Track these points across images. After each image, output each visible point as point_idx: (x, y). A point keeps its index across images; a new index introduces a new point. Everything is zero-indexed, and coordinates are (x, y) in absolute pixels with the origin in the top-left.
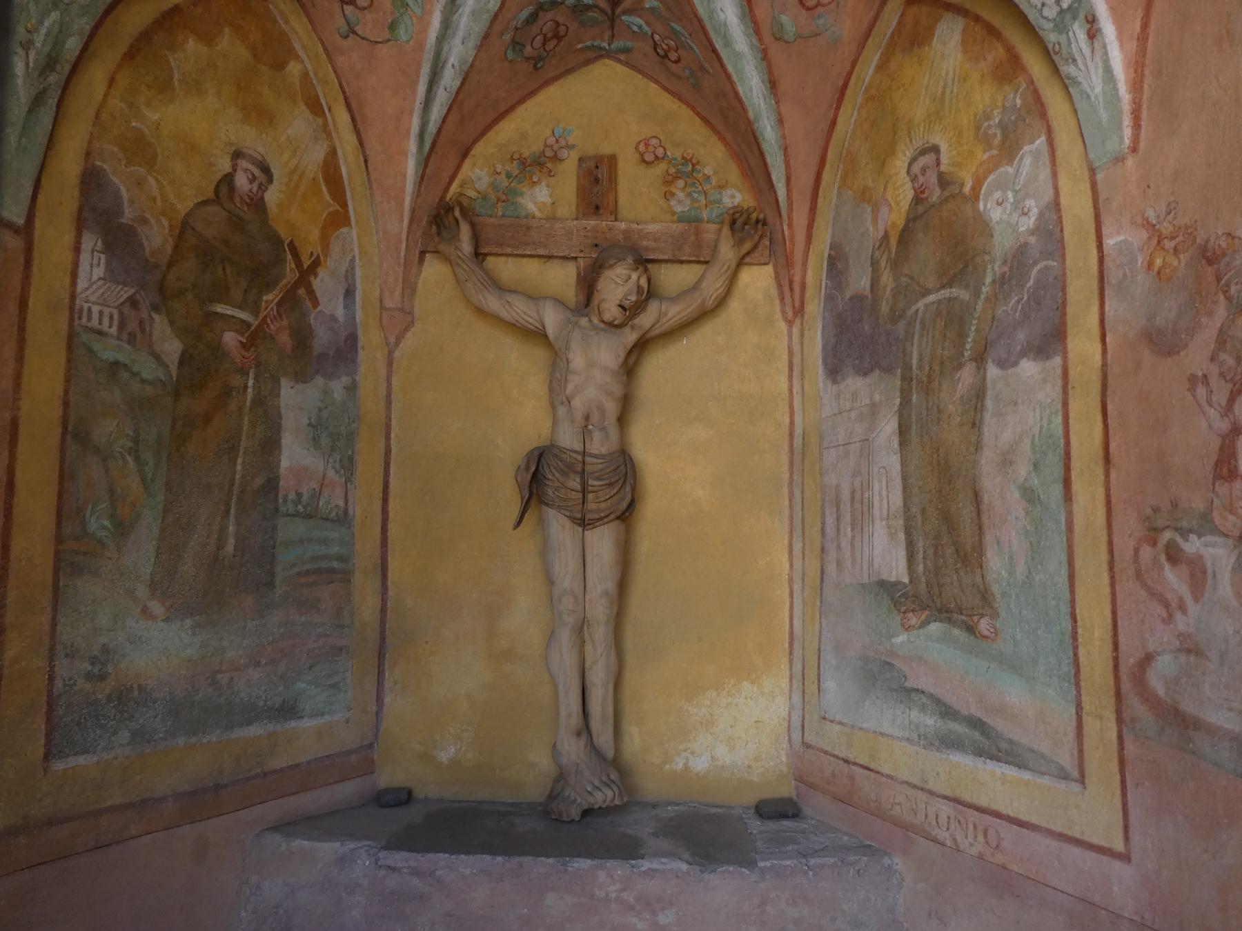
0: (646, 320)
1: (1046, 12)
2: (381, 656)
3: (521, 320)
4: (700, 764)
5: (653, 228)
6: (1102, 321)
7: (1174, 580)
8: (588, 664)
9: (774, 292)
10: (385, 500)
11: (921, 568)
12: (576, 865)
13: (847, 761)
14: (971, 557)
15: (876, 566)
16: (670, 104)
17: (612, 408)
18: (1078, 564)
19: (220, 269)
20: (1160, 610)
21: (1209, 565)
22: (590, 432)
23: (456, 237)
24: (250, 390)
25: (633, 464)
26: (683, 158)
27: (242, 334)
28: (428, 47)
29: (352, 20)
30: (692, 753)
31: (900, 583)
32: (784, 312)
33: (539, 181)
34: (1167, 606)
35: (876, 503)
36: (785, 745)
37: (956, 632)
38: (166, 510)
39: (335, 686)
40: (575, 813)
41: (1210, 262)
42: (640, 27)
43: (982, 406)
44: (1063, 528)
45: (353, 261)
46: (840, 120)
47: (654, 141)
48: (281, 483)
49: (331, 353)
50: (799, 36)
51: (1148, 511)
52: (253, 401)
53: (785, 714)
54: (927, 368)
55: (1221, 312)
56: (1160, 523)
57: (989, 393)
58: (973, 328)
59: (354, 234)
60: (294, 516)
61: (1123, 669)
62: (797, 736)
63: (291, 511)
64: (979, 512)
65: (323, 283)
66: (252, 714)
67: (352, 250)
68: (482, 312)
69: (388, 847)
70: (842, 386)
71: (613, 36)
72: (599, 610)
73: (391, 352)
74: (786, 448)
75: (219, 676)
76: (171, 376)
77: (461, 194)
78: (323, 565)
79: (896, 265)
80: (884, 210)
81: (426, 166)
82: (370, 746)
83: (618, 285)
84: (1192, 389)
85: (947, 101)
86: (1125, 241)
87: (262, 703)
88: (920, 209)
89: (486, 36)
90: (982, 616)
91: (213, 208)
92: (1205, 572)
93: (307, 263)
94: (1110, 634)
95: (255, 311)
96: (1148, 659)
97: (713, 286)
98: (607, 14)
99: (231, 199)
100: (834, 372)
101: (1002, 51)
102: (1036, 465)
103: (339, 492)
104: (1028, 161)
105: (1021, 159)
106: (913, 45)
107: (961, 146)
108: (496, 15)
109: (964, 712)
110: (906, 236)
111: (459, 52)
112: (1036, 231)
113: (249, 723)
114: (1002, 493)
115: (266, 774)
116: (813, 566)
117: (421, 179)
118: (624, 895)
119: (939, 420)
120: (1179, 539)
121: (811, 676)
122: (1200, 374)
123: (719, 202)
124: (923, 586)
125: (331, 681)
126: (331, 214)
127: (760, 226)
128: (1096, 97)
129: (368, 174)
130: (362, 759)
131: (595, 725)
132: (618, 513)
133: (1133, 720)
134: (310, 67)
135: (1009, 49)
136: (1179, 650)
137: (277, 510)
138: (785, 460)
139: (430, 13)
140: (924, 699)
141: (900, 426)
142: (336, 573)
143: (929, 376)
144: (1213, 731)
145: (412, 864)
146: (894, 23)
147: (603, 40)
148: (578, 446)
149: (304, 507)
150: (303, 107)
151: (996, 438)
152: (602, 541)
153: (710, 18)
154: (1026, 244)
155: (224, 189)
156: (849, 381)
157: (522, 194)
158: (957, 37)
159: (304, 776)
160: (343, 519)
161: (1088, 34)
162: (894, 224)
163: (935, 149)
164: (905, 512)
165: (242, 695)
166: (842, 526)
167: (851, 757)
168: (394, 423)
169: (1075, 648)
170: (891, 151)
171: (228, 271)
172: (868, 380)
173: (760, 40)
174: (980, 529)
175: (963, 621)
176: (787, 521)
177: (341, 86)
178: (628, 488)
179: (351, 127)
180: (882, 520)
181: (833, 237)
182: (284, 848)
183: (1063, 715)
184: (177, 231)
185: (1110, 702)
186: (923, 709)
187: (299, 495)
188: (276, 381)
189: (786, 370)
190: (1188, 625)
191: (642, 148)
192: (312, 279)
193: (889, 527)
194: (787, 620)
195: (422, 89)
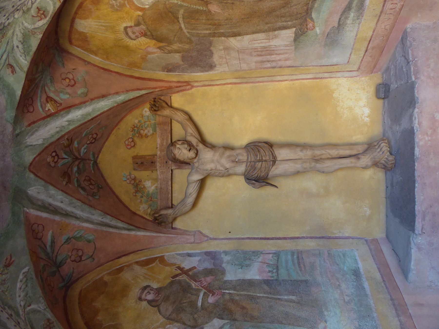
0: (194, 141)
2: (329, 238)
3: (196, 189)
4: (367, 111)
5: (159, 141)
8: (330, 157)
9: (181, 94)
10: (268, 239)
11: (290, 23)
12: (417, 154)
13: (366, 51)
15: (288, 43)
16: (112, 137)
17: (228, 153)
19: (184, 305)
22: (239, 160)
23: (166, 216)
24: (230, 292)
25: (250, 143)
26: (132, 131)
27: (209, 295)
28: (96, 228)
30: (363, 115)
31: (295, 32)
32: (188, 90)
33: (144, 185)
35: (263, 45)
36: (358, 78)
37: (316, 5)
38: (281, 323)
39: (344, 256)
40: (391, 158)
42: (85, 149)
45: (177, 254)
47: (127, 142)
48: (265, 278)
49: (213, 261)
50: (86, 87)
52: (235, 290)
53: (345, 79)
54: (210, 26)
58: (195, 7)
59: (167, 254)
60: (278, 273)
62: (355, 74)
63: (276, 275)
65: (187, 264)
66: (360, 287)
67: (173, 255)
68: (195, 204)
69: (413, 230)
70: (217, 63)
71: (89, 159)
72: (309, 153)
73: (211, 239)
74: (240, 85)
75: (346, 300)
76: (228, 322)
77: (150, 214)
78: (296, 261)
79: (170, 43)
80: (150, 49)
81: (139, 228)
82: (366, 241)
83: (182, 152)
87: (355, 283)
89: (91, 206)
91: (161, 308)
93: (179, 272)
95: (200, 290)
97: (180, 116)
99: (157, 301)
100: (211, 67)
103: (266, 256)
106: (87, 41)
108: (83, 202)
110: (159, 39)
111: (97, 217)
113: (363, 288)
115: (384, 281)
116: (287, 71)
117: (145, 229)
118: (429, 133)
119: (231, 19)
123: (148, 117)
125: (342, 257)
126: (160, 263)
127: (156, 100)
129: (144, 250)
130: (373, 244)
131: (354, 152)
132: (270, 148)
134: (105, 273)
137: (276, 280)
139: (83, 227)
140: (343, 18)
141: (232, 37)
142: (298, 256)
143: (213, 25)
145: (420, 220)
146: (79, 49)
147: (90, 163)
148: (244, 165)
149: (274, 269)
150: (121, 275)
152: (282, 154)
155: (154, 304)
156: (215, 60)
157: (148, 191)
158: (83, 22)
159: (383, 266)
160: (277, 254)
162: (154, 45)
163: (126, 28)
164: (267, 32)
165: (352, 291)
166: (271, 60)
167: (364, 49)
168: (238, 237)
170: (126, 48)
171: (185, 301)
172: (214, 52)
175: (312, 3)
176: (269, 83)
177: (112, 260)
178: (260, 144)
179: (127, 256)
180: (270, 42)
181: (159, 71)
182: (414, 272)
184: (171, 321)
186: (347, 18)
187: (269, 271)
188: (226, 282)
189: (210, 87)
191: (129, 147)
192: (185, 269)
193: (273, 39)
194: (308, 81)
195: (111, 230)
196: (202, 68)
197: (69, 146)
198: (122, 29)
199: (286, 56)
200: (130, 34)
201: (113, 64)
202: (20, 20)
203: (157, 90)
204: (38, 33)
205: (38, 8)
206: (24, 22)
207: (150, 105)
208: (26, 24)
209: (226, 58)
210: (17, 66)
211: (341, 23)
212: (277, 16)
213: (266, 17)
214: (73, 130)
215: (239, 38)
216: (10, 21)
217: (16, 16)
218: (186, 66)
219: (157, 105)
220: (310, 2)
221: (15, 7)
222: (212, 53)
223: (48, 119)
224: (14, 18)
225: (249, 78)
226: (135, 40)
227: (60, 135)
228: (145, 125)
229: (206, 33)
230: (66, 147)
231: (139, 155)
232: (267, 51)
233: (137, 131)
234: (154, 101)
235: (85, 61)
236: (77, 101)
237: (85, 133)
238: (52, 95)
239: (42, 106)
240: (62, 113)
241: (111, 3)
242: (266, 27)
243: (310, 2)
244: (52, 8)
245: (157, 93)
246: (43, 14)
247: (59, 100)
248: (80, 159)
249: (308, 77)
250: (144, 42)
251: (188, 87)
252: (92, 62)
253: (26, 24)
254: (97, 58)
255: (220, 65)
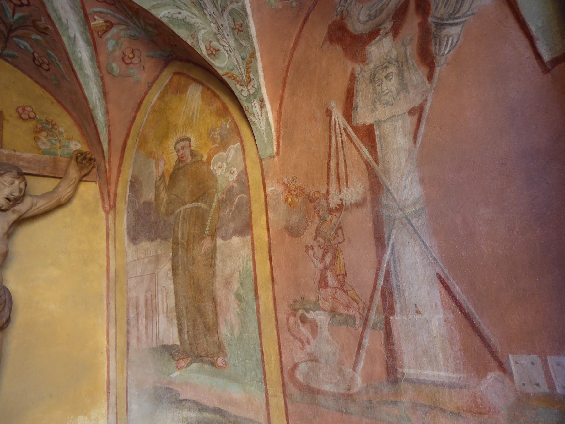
0: (23, 207)
1: (243, 93)
5: (26, 155)
6: (267, 222)
7: (304, 330)
9: (99, 196)
14: (212, 329)
15: (161, 336)
16: (38, 90)
18: (263, 327)
20: (299, 344)
21: (319, 323)
32: (104, 207)
34: (302, 342)
37: (206, 366)
41: (311, 202)
42: (26, 47)
43: (215, 257)
44: (255, 311)
47: (28, 109)
51: (292, 302)
54: (186, 239)
55: (317, 221)
56: (297, 307)
57: (218, 251)
58: (209, 221)
61: (285, 373)
64: (215, 307)
70: (139, 246)
74: (105, 278)
79: (169, 189)
80: (162, 164)
84: (307, 251)
86: (275, 190)
88: (181, 165)
90: (219, 356)
92: (317, 326)
94: (278, 357)
96: (296, 366)
98: (4, 34)
100: (134, 239)
102: (242, 284)
104: (232, 151)
105: (230, 151)
106: (177, 92)
109: (211, 406)
110: (174, 177)
112: (237, 181)
114: (227, 298)
116: (122, 341)
119: (193, 263)
120: (305, 313)
121: (122, 404)
122: (310, 245)
123: (68, 147)
124: (187, 346)
127: (93, 162)
133: (291, 395)
136: (308, 361)
138: (104, 285)
140: (189, 403)
141: (172, 266)
144: (325, 393)
146: (168, 81)
151: (223, 272)
153: (73, 54)
154: (232, 186)
162: (167, 170)
163: (189, 140)
164: (176, 309)
169: (263, 366)
170: (166, 136)
172: (154, 243)
173: (100, 71)
174: (216, 315)
175: (209, 361)
178: (7, 310)
181: (133, 172)
183: (259, 398)
185: (280, 389)
186: (189, 409)
190: (311, 349)
191: (20, 110)
193: (167, 317)
194: (106, 374)
196: (134, 227)
197: (36, 27)
198: (189, 135)
199: (144, 338)
200: (182, 144)
201: (147, 116)
202: (208, 27)
203: (107, 165)
204: (192, 41)
205: (219, 50)
206: (206, 31)
207: (86, 152)
208: (203, 32)
209: (145, 258)
210: (158, 4)
211: (184, 403)
212: (195, 320)
213: (194, 306)
214: (60, 39)
215: (170, 274)
216: (208, 16)
217: (212, 25)
218: (138, 207)
219: (84, 162)
220: (210, 359)
221: (221, 27)
222: (152, 241)
223: (82, 14)
224: (211, 22)
225: (116, 289)
226: (175, 147)
227: (55, 21)
228: (55, 140)
229: (178, 234)
230: (34, 22)
231: (5, 122)
232: (152, 311)
233: (47, 127)
234: (91, 159)
235: (153, 82)
236: (102, 58)
237: (53, 54)
238: (114, 30)
239: (101, 12)
240: (89, 35)
241: (217, 129)
242: (182, 308)
243: (210, 359)
244: (218, 65)
245: (103, 164)
246: (212, 53)
247: (106, 37)
248: (8, 35)
249: (110, 374)
250: (171, 158)
251: (107, 207)
252: (150, 92)
253: (203, 32)
254: (155, 99)
255: (137, 251)
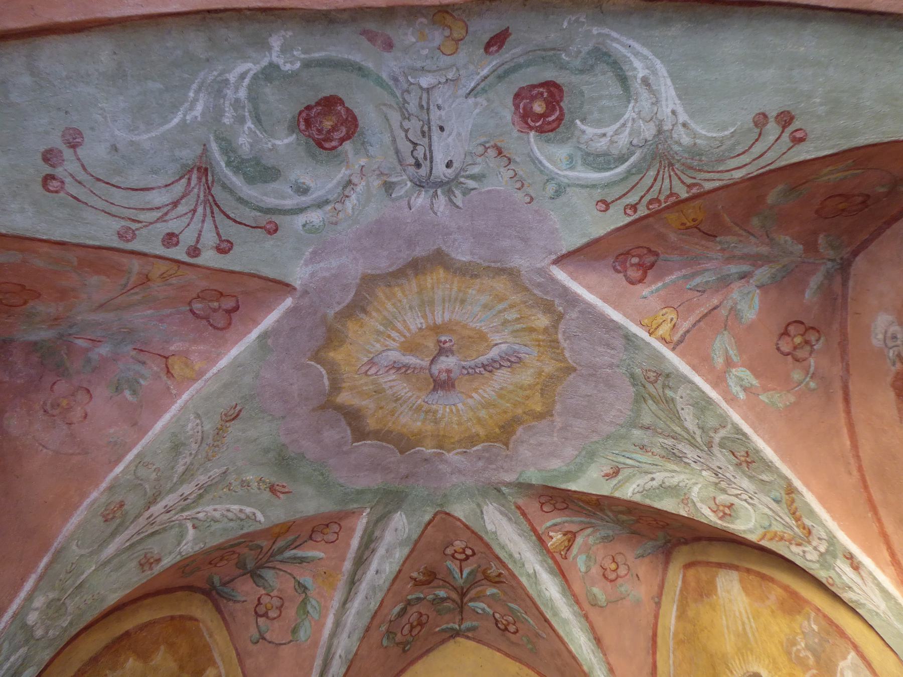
28: (322, 643)
29: (263, 628)
42: (483, 610)
46: (660, 664)
50: (609, 602)
85: (750, 635)
89: (368, 629)
101: (780, 591)
107: (780, 670)
108: (376, 613)
111: (345, 645)
128: (884, 613)
135: (786, 588)
139: (326, 616)
146: (680, 583)
153: (539, 596)
161: (853, 567)
173: (581, 608)
